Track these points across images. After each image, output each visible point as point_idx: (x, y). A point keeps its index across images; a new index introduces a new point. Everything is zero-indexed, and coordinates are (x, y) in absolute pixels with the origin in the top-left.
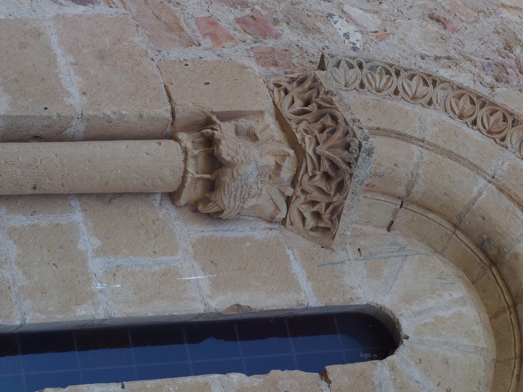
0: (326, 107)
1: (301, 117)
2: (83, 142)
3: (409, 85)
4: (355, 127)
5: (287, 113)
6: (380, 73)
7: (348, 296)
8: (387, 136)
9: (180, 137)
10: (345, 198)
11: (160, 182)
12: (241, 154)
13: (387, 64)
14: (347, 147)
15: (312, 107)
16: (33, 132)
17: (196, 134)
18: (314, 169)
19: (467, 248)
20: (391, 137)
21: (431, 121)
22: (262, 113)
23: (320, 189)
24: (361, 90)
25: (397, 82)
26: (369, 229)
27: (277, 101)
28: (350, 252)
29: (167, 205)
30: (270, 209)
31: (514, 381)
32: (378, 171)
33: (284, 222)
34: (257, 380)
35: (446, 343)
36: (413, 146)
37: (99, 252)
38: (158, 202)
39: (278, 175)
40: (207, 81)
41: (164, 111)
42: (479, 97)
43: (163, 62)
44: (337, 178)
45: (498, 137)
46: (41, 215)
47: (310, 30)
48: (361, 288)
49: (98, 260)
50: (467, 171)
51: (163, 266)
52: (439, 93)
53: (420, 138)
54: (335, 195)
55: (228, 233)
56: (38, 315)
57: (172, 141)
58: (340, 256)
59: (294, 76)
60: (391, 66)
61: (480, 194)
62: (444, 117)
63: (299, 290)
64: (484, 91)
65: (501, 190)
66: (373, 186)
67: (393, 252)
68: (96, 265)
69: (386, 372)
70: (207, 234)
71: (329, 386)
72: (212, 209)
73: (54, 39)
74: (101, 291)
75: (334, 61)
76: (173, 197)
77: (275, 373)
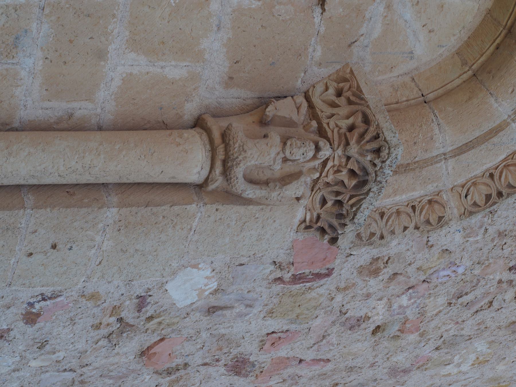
31: (492, 48)
71: (322, 14)
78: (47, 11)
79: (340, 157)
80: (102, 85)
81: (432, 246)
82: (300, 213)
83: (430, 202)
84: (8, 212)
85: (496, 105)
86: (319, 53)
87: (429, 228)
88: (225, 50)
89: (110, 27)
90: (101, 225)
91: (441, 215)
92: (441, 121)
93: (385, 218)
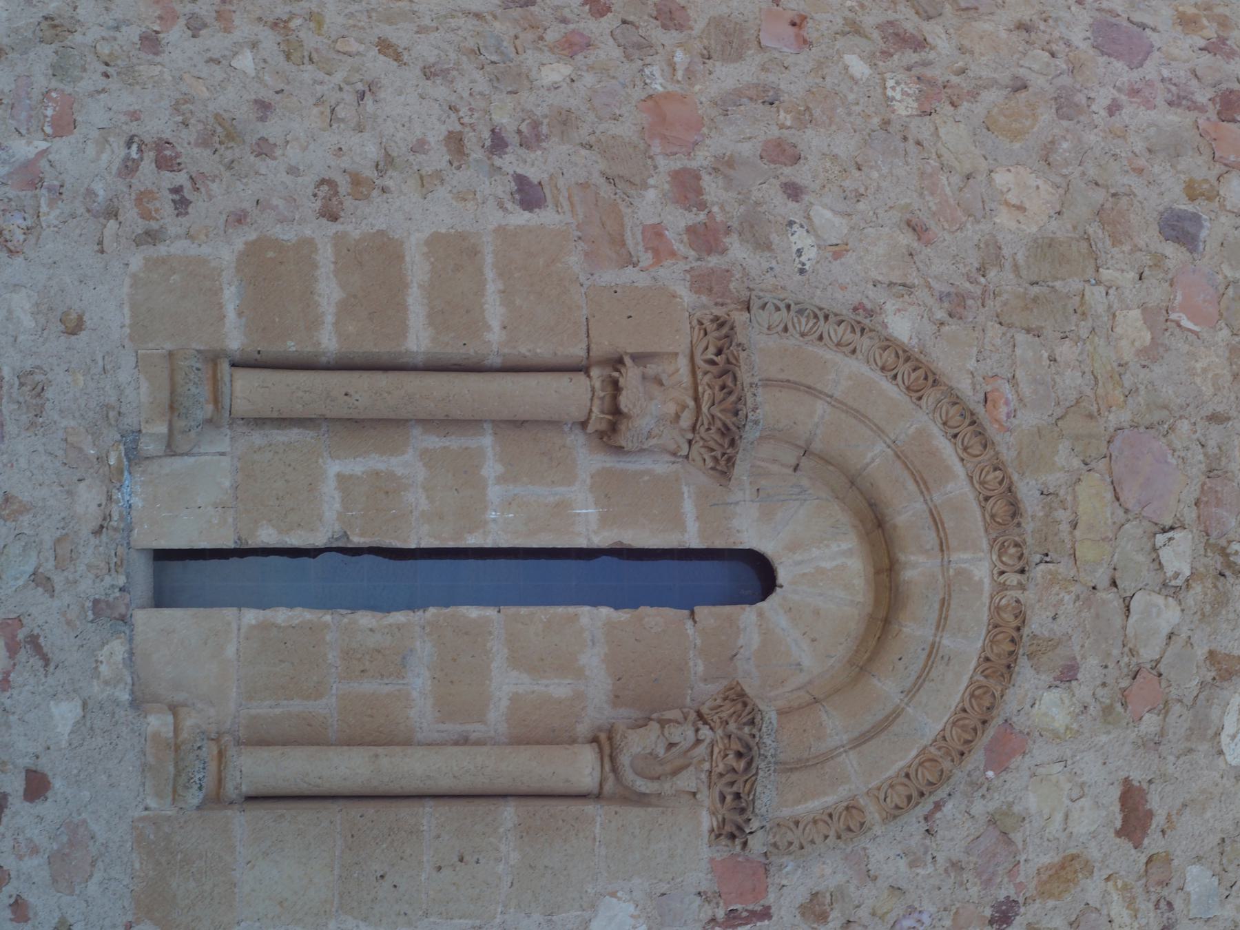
3: (835, 331)
5: (699, 361)
6: (808, 317)
14: (736, 414)
21: (847, 371)
25: (823, 327)
26: (775, 468)
29: (577, 431)
30: (673, 447)
33: (687, 457)
34: (624, 615)
35: (821, 595)
37: (501, 479)
44: (730, 436)
47: (764, 246)
48: (748, 534)
52: (865, 343)
56: (432, 540)
60: (821, 309)
61: (873, 460)
62: (865, 369)
65: (899, 457)
68: (494, 492)
69: (754, 617)
70: (608, 465)
73: (489, 259)
74: (494, 520)
75: (761, 302)
77: (644, 610)
78: (428, 629)
81: (876, 878)
82: (706, 821)
83: (847, 808)
85: (879, 684)
86: (701, 668)
87: (851, 835)
89: (489, 645)
90: (501, 830)
93: (801, 826)
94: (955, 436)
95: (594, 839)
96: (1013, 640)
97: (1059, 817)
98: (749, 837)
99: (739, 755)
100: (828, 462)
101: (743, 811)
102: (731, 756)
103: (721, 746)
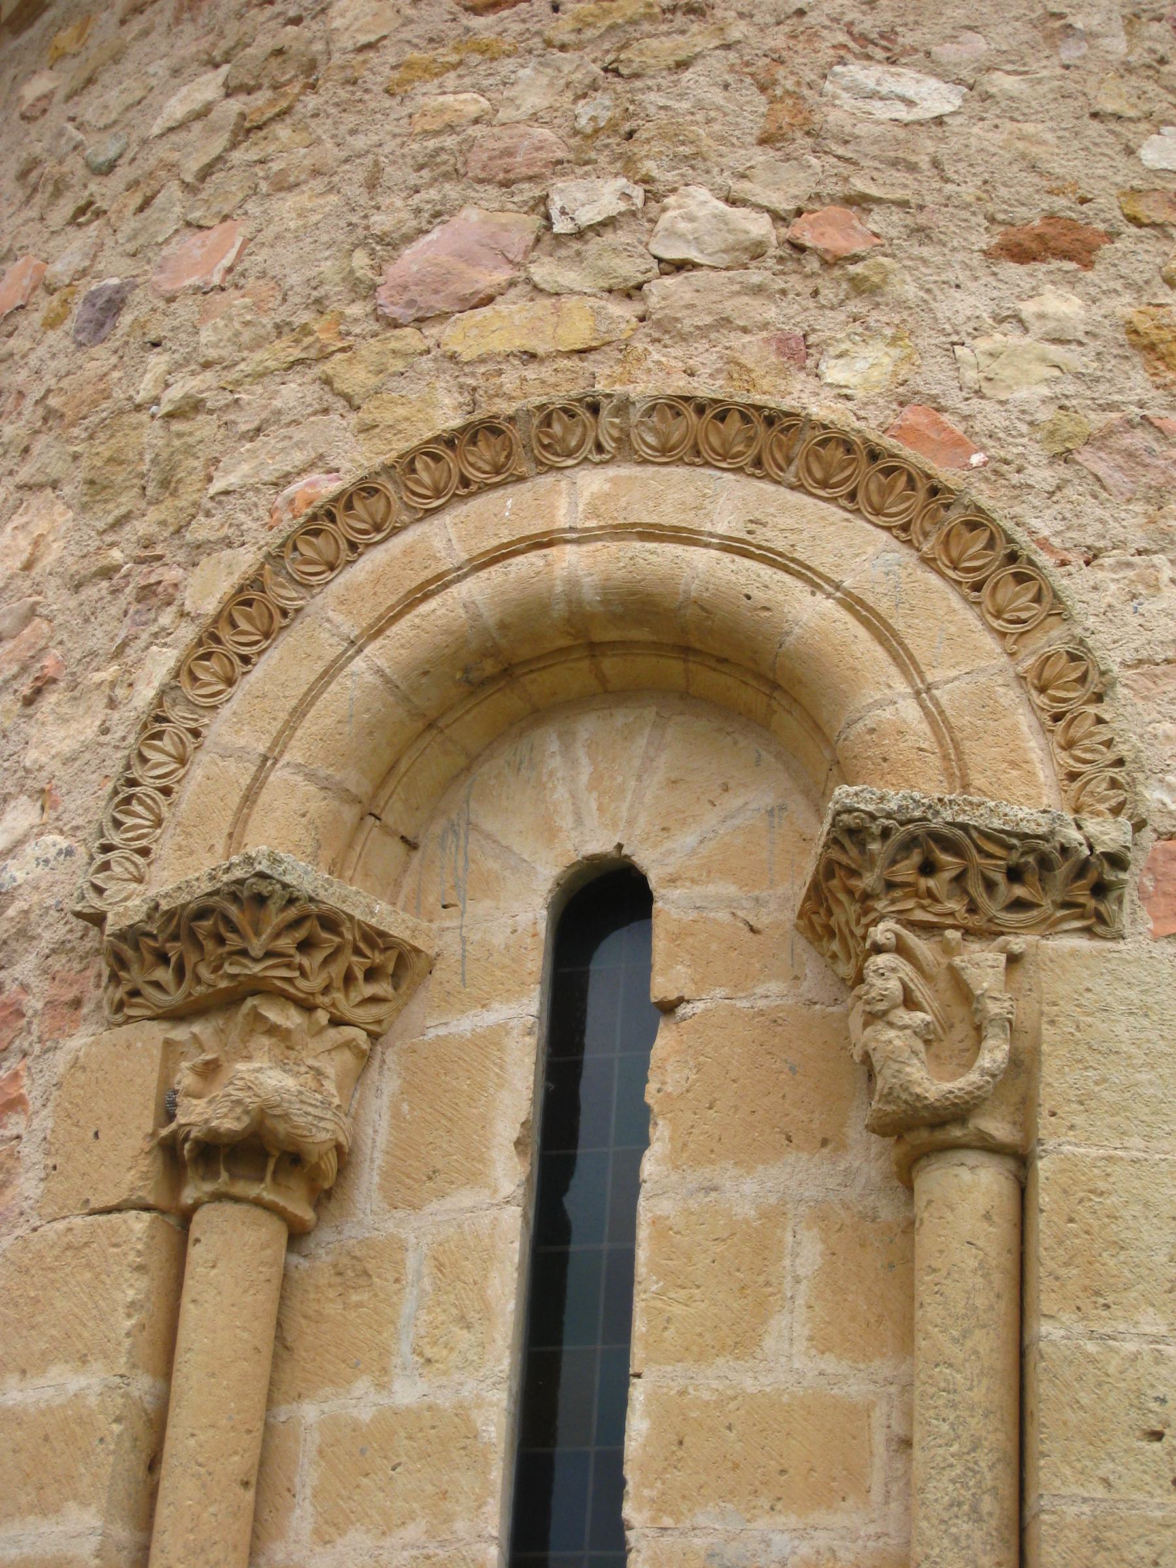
0: (178, 925)
1: (188, 975)
2: (173, 1382)
4: (225, 878)
5: (175, 997)
7: (529, 941)
8: (246, 822)
9: (190, 1201)
10: (351, 918)
11: (269, 1252)
12: (241, 1094)
13: (111, 799)
15: (174, 950)
16: (141, 1472)
17: (190, 1172)
18: (289, 966)
19: (473, 713)
20: (249, 815)
22: (168, 1043)
23: (326, 962)
24: (152, 856)
27: (148, 1013)
28: (447, 924)
29: (311, 1243)
32: (309, 850)
33: (374, 1037)
34: (661, 1135)
36: (271, 778)
38: (302, 1260)
39: (288, 1032)
40: (91, 1134)
41: (138, 1224)
42: (200, 643)
43: (43, 1212)
45: (279, 621)
46: (297, 1480)
48: (519, 918)
49: (396, 1386)
50: (334, 687)
51: (425, 1271)
53: (258, 762)
54: (340, 935)
55: (378, 1140)
57: (196, 1217)
58: (449, 945)
59: (106, 973)
60: (116, 792)
63: (503, 1028)
64: (188, 633)
65: (380, 632)
66: (334, 863)
67: (457, 847)
68: (407, 1392)
69: (676, 893)
72: (330, 1164)
75: (91, 895)
76: (297, 1236)
78: (668, 1521)
79: (893, 902)
80: (836, 1391)
83: (1042, 690)
84: (1044, 1545)
86: (774, 987)
87: (1093, 676)
88: (760, 1167)
89: (706, 1396)
91: (1065, 656)
92: (843, 724)
93: (1079, 767)
94: (353, 546)
95: (1109, 1159)
96: (722, 417)
97: (1056, 352)
98: (1099, 849)
99: (928, 868)
100: (392, 768)
101: (1045, 863)
102: (931, 883)
103: (910, 904)
